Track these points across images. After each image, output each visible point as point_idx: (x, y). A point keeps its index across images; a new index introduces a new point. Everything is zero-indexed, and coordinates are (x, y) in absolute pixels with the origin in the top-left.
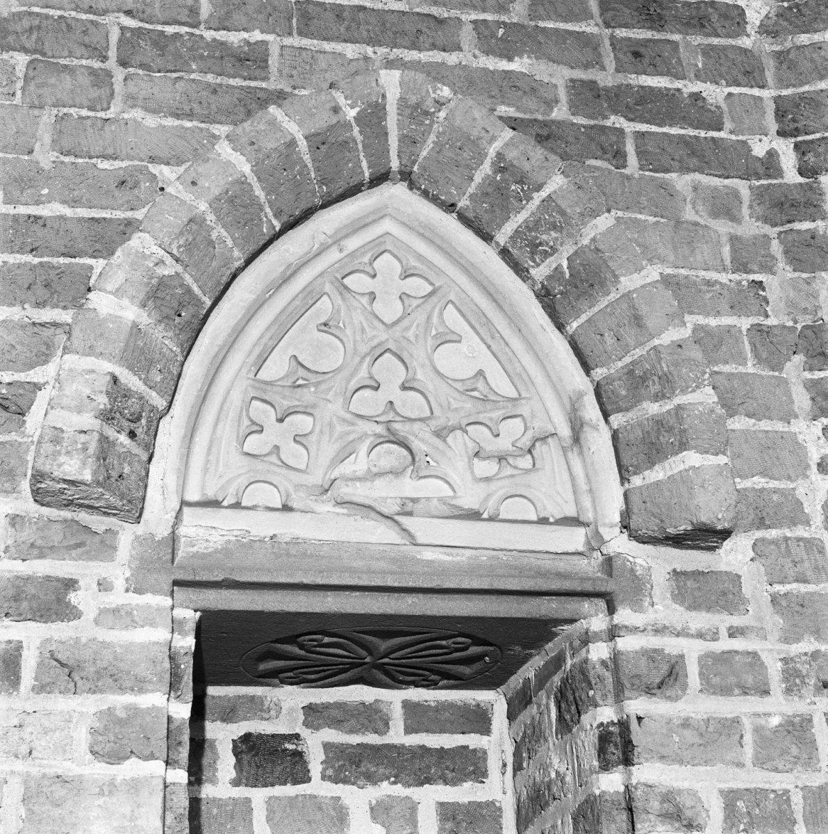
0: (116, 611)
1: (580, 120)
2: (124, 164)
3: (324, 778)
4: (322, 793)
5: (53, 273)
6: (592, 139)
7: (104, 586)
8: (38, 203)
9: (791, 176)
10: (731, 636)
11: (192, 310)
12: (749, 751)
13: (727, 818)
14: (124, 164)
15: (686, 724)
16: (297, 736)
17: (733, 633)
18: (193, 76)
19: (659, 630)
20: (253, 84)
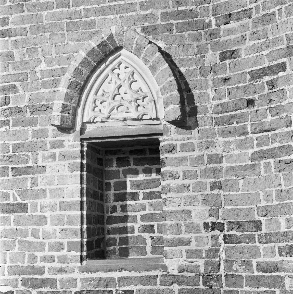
0: (71, 145)
1: (163, 23)
2: (68, 54)
3: (133, 165)
4: (133, 168)
5: (56, 80)
6: (165, 28)
7: (69, 140)
8: (53, 66)
9: (214, 27)
10: (188, 139)
11: (79, 86)
12: (189, 163)
13: (183, 176)
14: (68, 54)
15: (176, 158)
16: (128, 157)
17: (188, 139)
18: (80, 31)
19: (172, 140)
20: (92, 30)
